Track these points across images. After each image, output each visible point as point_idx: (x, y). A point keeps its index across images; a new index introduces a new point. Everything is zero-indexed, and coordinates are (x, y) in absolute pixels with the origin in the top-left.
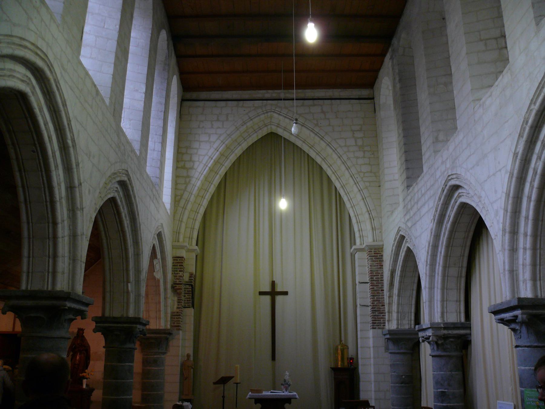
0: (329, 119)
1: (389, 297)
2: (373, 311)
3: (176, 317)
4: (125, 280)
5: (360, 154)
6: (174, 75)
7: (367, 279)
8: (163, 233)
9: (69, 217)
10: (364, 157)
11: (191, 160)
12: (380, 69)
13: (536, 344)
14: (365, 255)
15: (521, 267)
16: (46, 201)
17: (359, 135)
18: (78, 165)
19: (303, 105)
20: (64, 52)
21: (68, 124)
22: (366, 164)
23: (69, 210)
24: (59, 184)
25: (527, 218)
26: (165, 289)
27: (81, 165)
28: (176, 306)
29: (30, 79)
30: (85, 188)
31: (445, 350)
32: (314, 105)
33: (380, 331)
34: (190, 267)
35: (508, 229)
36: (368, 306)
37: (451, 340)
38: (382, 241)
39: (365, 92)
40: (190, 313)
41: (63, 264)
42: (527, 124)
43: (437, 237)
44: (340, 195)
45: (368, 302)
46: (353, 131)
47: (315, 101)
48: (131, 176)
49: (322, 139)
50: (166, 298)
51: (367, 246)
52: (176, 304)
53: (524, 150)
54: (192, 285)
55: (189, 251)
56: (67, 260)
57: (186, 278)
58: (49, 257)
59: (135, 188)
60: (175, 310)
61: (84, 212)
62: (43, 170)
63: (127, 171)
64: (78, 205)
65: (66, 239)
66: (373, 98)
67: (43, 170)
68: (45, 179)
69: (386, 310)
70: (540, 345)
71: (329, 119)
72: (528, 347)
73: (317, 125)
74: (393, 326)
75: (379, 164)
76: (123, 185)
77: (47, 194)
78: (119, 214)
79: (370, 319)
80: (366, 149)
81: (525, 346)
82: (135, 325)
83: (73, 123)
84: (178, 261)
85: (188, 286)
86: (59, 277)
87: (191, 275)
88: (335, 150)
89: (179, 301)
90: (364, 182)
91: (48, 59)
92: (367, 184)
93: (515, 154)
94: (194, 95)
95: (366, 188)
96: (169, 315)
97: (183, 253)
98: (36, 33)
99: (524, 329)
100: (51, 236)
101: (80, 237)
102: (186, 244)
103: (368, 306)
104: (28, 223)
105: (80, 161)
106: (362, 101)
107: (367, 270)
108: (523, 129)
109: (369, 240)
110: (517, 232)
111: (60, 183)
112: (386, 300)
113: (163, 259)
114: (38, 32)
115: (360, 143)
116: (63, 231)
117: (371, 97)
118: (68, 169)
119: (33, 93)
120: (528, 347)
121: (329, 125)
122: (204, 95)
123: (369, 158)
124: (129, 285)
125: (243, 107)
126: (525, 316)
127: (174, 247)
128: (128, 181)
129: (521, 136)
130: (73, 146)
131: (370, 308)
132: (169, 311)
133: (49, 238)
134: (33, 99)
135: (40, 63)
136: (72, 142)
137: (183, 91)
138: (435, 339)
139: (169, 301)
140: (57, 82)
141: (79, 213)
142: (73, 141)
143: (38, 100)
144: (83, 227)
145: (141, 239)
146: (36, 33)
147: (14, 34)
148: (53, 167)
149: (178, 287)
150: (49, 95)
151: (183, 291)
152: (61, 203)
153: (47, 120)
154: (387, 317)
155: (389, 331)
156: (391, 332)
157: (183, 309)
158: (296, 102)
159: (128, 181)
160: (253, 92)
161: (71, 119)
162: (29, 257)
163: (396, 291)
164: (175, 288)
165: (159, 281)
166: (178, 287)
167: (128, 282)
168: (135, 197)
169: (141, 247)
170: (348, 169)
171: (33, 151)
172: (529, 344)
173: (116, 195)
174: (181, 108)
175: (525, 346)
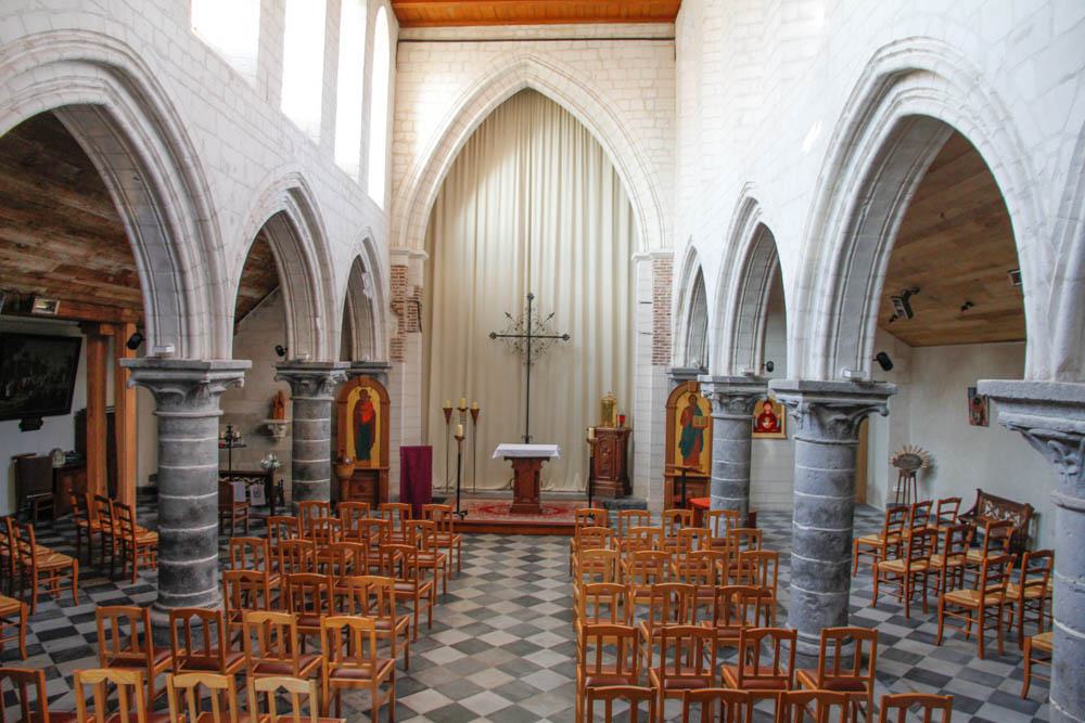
0: (607, 70)
1: (677, 324)
2: (656, 342)
3: (397, 345)
4: (312, 314)
5: (650, 123)
6: (377, 10)
7: (650, 298)
8: (372, 242)
9: (203, 260)
10: (654, 127)
11: (413, 131)
12: (677, 13)
13: (818, 440)
14: (649, 265)
15: (813, 336)
16: (166, 243)
17: (650, 93)
18: (207, 189)
19: (571, 49)
20: (161, 31)
21: (183, 137)
22: (657, 138)
23: (201, 250)
24: (182, 220)
25: (827, 270)
26: (382, 310)
27: (212, 189)
28: (396, 332)
29: (106, 82)
30: (224, 218)
31: (730, 411)
32: (588, 48)
33: (663, 368)
34: (418, 278)
35: (801, 283)
36: (649, 334)
37: (739, 399)
38: (672, 247)
39: (661, 29)
40: (415, 342)
41: (200, 323)
42: (837, 138)
43: (730, 262)
44: (619, 178)
45: (650, 328)
46: (641, 88)
47: (589, 42)
48: (307, 178)
49: (597, 99)
50: (383, 321)
51: (653, 254)
52: (397, 328)
53: (831, 176)
54: (418, 303)
55: (414, 257)
56: (205, 317)
57: (411, 294)
58: (180, 316)
59: (315, 194)
60: (396, 336)
61: (226, 252)
62: (155, 203)
63: (299, 173)
64: (215, 244)
65: (203, 290)
66: (674, 39)
67: (155, 203)
68: (159, 213)
69: (673, 340)
70: (824, 441)
71: (607, 70)
72: (809, 441)
73: (590, 78)
74: (678, 362)
75: (675, 139)
76: (295, 192)
77: (166, 233)
78: (293, 229)
79: (651, 351)
80: (658, 115)
81: (806, 441)
82: (327, 372)
83: (191, 133)
84: (399, 272)
85: (412, 304)
86: (197, 341)
87: (417, 289)
88: (614, 116)
89: (401, 324)
90: (653, 163)
91: (131, 49)
92: (657, 166)
93: (820, 179)
94: (416, 33)
95: (656, 172)
96: (388, 343)
97: (404, 260)
98: (100, 15)
99: (806, 417)
100: (179, 287)
101: (221, 286)
102: (408, 249)
103: (649, 334)
104: (147, 270)
105: (209, 182)
106: (656, 42)
107: (650, 285)
108: (831, 145)
109: (655, 246)
110: (814, 287)
111: (184, 218)
112: (673, 330)
113: (376, 271)
114: (104, 13)
115: (650, 104)
116: (196, 281)
117: (670, 35)
118: (192, 196)
119: (115, 102)
120: (809, 441)
121: (608, 79)
122: (429, 32)
123: (662, 129)
124: (318, 320)
125: (485, 51)
126: (807, 405)
127: (392, 253)
128: (302, 187)
129: (828, 153)
130: (195, 165)
131: (652, 336)
132: (388, 339)
133: (177, 291)
134: (118, 112)
135: (116, 59)
136: (193, 160)
137: (400, 27)
138: (717, 397)
139: (388, 325)
140: (153, 80)
141: (217, 255)
142: (195, 157)
143: (127, 111)
144: (226, 271)
145: (331, 259)
146: (100, 15)
147: (55, 28)
148: (167, 198)
149: (398, 305)
150: (143, 99)
151: (405, 312)
152: (188, 244)
153: (146, 134)
154: (672, 350)
155: (673, 370)
156: (675, 372)
157: (406, 334)
158: (213, 497)
159: (302, 187)
160: (501, 27)
161: (186, 127)
162: (154, 315)
163: (685, 318)
164: (395, 308)
165: (370, 301)
166: (398, 305)
167: (316, 316)
168: (316, 205)
169: (331, 270)
170: (631, 144)
171: (135, 178)
172: (810, 439)
173: (285, 207)
174: (397, 51)
175: (806, 441)
